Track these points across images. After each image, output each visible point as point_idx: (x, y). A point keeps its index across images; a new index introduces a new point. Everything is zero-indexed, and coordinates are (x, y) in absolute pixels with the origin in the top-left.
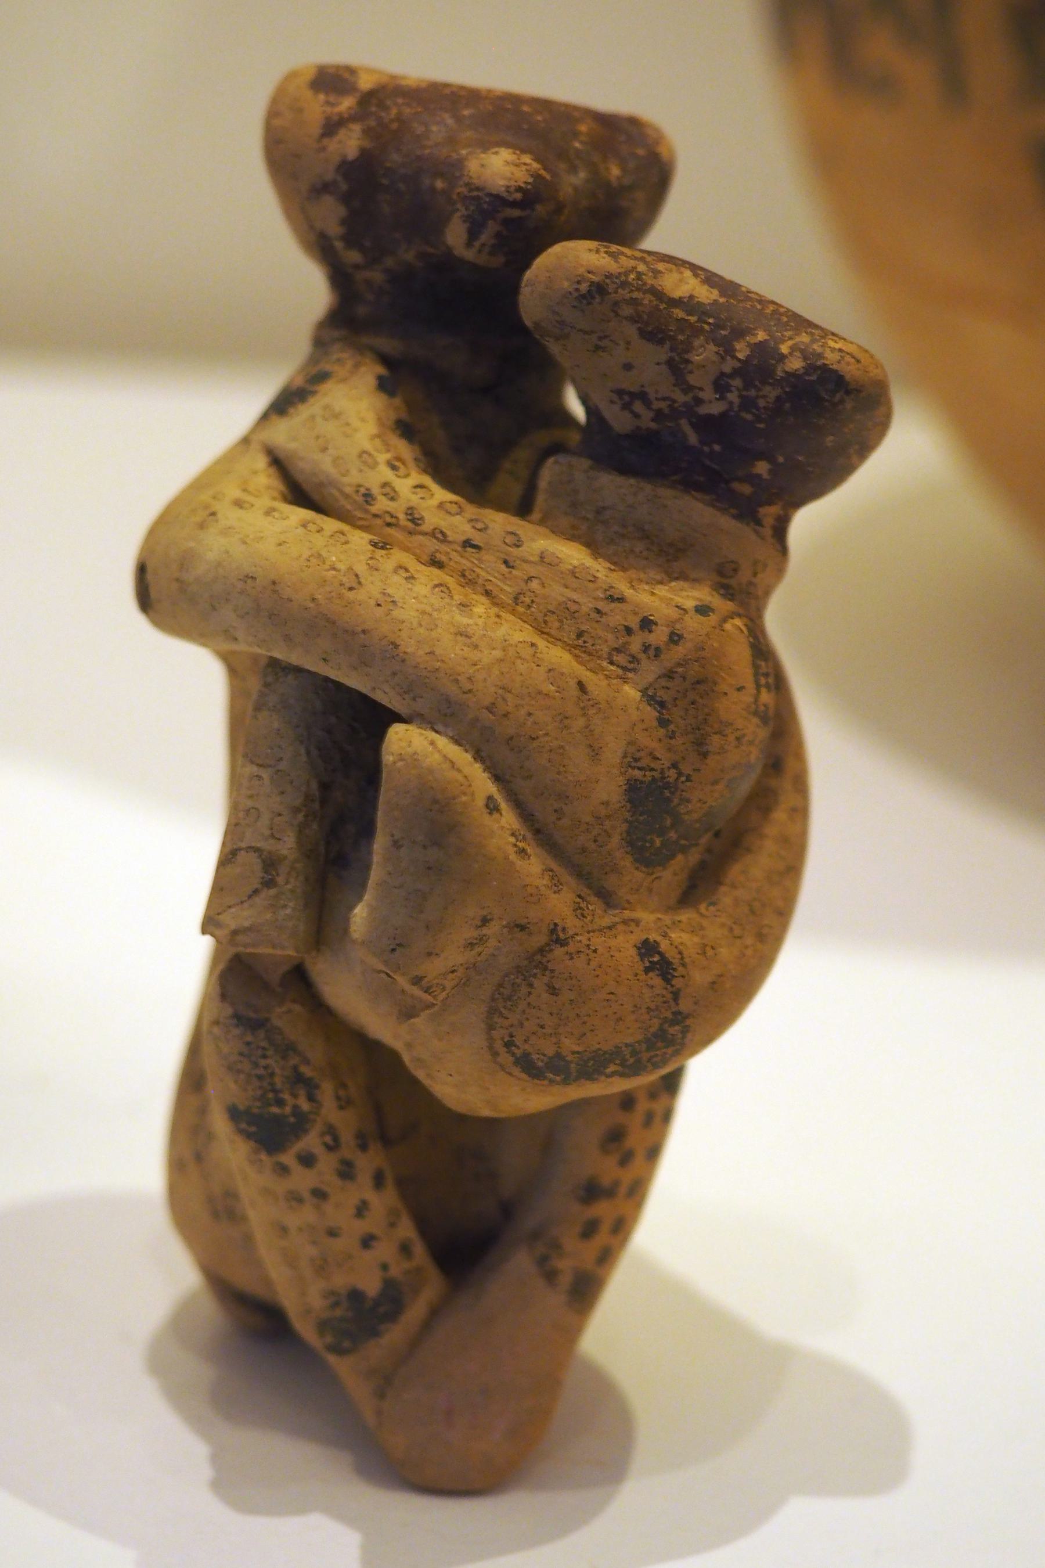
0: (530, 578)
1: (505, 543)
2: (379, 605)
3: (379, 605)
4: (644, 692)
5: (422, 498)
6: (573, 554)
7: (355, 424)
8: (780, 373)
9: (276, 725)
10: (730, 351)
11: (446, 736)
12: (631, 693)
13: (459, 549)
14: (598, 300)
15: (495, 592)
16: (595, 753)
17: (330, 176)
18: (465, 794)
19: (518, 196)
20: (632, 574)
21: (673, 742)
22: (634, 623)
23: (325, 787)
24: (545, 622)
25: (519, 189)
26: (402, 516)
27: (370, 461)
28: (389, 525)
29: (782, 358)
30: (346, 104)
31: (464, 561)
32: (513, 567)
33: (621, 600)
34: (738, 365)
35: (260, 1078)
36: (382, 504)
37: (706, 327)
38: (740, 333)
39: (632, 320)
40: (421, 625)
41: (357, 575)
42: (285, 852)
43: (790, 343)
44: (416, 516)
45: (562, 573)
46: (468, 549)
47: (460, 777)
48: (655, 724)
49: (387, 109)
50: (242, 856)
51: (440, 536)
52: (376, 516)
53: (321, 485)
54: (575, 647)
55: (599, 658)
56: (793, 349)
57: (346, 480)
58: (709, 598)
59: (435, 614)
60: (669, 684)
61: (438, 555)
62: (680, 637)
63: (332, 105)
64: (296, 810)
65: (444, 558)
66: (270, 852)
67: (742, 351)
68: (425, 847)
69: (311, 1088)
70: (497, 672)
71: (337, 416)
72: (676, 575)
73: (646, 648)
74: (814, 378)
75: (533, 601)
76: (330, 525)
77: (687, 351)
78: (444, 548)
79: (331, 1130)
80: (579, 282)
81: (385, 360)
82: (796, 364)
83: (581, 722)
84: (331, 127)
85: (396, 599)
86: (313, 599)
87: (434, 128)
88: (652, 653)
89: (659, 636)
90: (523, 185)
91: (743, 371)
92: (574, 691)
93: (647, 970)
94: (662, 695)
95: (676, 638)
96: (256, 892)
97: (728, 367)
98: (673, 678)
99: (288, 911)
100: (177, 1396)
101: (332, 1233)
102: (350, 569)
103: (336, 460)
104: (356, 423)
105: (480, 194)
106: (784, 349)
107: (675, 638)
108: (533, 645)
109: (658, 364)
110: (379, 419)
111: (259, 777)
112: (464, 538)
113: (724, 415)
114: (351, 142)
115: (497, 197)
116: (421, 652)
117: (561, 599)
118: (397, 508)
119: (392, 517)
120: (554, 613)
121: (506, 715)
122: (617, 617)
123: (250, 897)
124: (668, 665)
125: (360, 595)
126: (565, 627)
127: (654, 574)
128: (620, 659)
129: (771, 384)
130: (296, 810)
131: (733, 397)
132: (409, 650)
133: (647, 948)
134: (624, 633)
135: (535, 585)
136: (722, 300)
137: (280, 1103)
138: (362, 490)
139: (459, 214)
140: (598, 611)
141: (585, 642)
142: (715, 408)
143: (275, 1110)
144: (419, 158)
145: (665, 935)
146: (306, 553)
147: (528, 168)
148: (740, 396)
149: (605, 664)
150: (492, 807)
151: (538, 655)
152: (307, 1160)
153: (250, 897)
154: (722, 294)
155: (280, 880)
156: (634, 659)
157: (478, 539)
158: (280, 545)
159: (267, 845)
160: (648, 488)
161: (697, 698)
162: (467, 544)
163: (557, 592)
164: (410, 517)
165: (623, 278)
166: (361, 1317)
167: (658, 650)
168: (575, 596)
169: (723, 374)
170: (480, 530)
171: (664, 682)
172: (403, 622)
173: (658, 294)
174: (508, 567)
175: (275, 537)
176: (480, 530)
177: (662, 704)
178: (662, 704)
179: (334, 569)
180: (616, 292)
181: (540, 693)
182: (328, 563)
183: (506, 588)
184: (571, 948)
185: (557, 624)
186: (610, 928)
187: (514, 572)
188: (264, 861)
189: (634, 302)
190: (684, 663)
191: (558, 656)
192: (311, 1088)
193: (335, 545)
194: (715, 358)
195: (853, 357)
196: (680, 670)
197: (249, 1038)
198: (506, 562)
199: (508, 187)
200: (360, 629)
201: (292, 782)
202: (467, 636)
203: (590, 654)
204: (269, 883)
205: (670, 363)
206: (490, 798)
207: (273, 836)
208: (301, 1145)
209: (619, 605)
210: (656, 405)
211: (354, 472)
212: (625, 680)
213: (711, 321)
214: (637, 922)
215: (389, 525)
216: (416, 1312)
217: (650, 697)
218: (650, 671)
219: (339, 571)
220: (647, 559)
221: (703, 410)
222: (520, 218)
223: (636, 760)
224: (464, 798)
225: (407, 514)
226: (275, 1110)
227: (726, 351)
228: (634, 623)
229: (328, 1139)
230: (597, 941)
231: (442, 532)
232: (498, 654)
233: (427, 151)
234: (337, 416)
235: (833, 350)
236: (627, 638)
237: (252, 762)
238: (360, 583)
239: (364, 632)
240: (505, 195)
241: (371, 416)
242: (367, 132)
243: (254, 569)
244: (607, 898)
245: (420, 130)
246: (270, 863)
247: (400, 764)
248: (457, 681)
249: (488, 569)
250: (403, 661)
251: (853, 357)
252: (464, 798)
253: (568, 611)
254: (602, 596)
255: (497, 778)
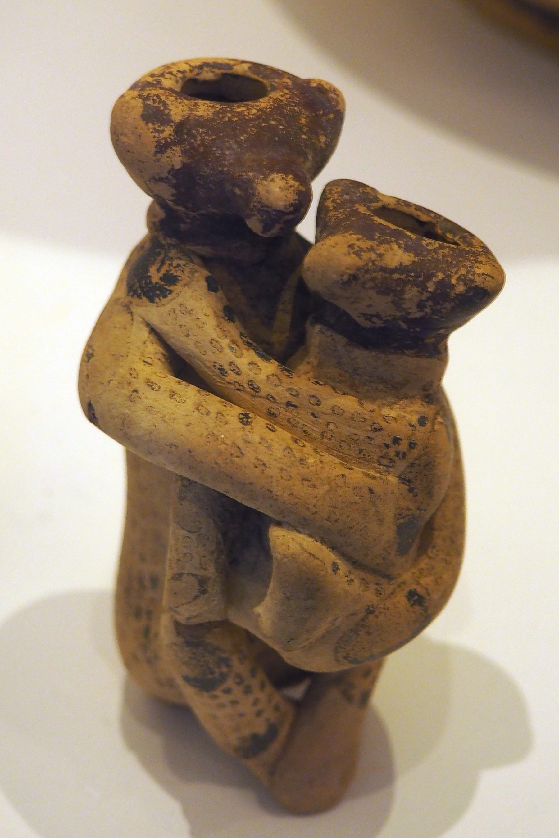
0: (329, 424)
1: (310, 403)
2: (256, 467)
3: (256, 467)
4: (399, 477)
5: (255, 374)
6: (348, 403)
7: (194, 311)
8: (453, 295)
9: (195, 510)
10: (425, 289)
11: (305, 534)
12: (393, 479)
13: (284, 407)
14: (354, 283)
15: (309, 431)
16: (381, 521)
17: (164, 175)
18: (323, 570)
19: (291, 209)
20: (379, 402)
21: (417, 498)
22: (389, 441)
23: (224, 534)
24: (341, 447)
25: (292, 205)
26: (246, 386)
27: (217, 346)
28: (238, 390)
29: (453, 286)
30: (168, 132)
31: (288, 414)
32: (317, 417)
33: (381, 429)
34: (429, 295)
35: (202, 666)
36: (232, 377)
37: (411, 279)
38: (429, 277)
39: (373, 288)
40: (282, 478)
41: (239, 448)
42: (210, 575)
43: (456, 276)
44: (255, 386)
45: (346, 419)
46: (290, 407)
47: (319, 563)
48: (408, 492)
49: (194, 137)
50: (185, 578)
51: (271, 399)
52: (229, 383)
53: (189, 355)
54: (359, 458)
55: (373, 462)
56: (458, 279)
57: (205, 357)
58: (423, 409)
59: (289, 469)
60: (413, 470)
61: (272, 410)
62: (415, 444)
63: (158, 131)
64: (212, 553)
65: (276, 412)
66: (202, 576)
67: (431, 287)
68: (304, 600)
69: (226, 662)
70: (328, 499)
71: (190, 312)
72: (402, 397)
73: (398, 454)
74: (471, 294)
75: (332, 436)
76: (213, 403)
77: (403, 294)
78: (275, 406)
79: (239, 676)
80: (342, 275)
81: (206, 261)
82: (461, 288)
83: (373, 510)
84: (162, 147)
85: (266, 463)
86: (216, 463)
87: (227, 152)
88: (401, 456)
89: (403, 446)
90: (294, 202)
91: (434, 297)
92: (368, 495)
93: (412, 606)
94: (411, 476)
95: (413, 445)
96: (197, 597)
97: (425, 296)
98: (414, 467)
99: (215, 602)
100: (147, 763)
101: (241, 715)
102: (234, 443)
103: (196, 343)
104: (203, 318)
105: (269, 209)
106: (454, 281)
107: (412, 445)
108: (343, 475)
109: (387, 303)
110: (215, 313)
111: (190, 538)
112: (286, 401)
113: (422, 318)
114: (175, 158)
115: (280, 211)
116: (285, 495)
117: (348, 434)
118: (243, 380)
119: (240, 385)
120: (345, 441)
121: (336, 521)
122: (379, 439)
123: (194, 599)
124: (410, 461)
125: (244, 461)
126: (352, 448)
127: (391, 399)
128: (385, 462)
129: (448, 302)
130: (212, 553)
131: (428, 310)
132: (278, 494)
133: (412, 594)
134: (385, 447)
135: (332, 427)
136: (416, 259)
137: (212, 673)
138: (218, 366)
139: (254, 218)
140: (369, 438)
141: (364, 455)
142: (418, 315)
143: (210, 676)
144: (221, 172)
145: (418, 584)
146: (205, 434)
147: (293, 189)
148: (432, 309)
149: (376, 465)
150: (335, 568)
151: (347, 481)
152: (228, 691)
153: (194, 599)
154: (416, 255)
155: (209, 589)
156: (392, 461)
157: (294, 401)
158: (188, 426)
159: (201, 573)
160: (383, 356)
161: (427, 473)
162: (289, 404)
163: (345, 430)
164: (251, 387)
165: (366, 268)
166: (255, 746)
167: (404, 454)
168: (356, 431)
169: (422, 300)
170: (294, 396)
171: (408, 470)
172: (272, 477)
173: (384, 269)
174: (315, 417)
175: (178, 410)
176: (294, 396)
177: (409, 481)
178: (409, 481)
179: (225, 443)
180: (363, 277)
181: (351, 503)
182: (220, 440)
183: (315, 429)
184: (376, 613)
185: (347, 447)
186: (392, 593)
187: (319, 420)
188: (199, 581)
189: (373, 279)
190: (419, 458)
191: (357, 475)
192: (226, 662)
193: (220, 426)
194: (417, 294)
195: (490, 276)
196: (417, 462)
197: (195, 650)
198: (313, 414)
199: (285, 206)
200: (247, 482)
201: (208, 539)
202: (309, 481)
203: (367, 461)
204: (204, 592)
205: (393, 302)
206: (334, 564)
207: (202, 568)
208: (225, 686)
209: (380, 433)
210: (385, 319)
211: (209, 353)
212: (388, 473)
213: (413, 274)
214: (404, 583)
215: (238, 390)
216: (283, 732)
217: (403, 480)
218: (401, 465)
219: (227, 445)
220: (386, 392)
221: (410, 317)
222: (293, 218)
223: (400, 515)
224: (323, 573)
225: (249, 385)
226: (210, 676)
227: (423, 290)
228: (389, 441)
229: (238, 680)
230: (389, 604)
231: (272, 397)
232: (326, 487)
233: (225, 169)
234: (190, 312)
235: (479, 275)
236: (387, 450)
237: (183, 528)
238: (241, 453)
239: (250, 484)
240: (285, 210)
241: (209, 311)
242: (184, 152)
243: (175, 441)
244: (389, 578)
245: (218, 153)
246: (203, 582)
247: (285, 560)
248: (308, 508)
249: (304, 419)
250: (276, 500)
251: (490, 276)
252: (323, 573)
253: (352, 440)
254: (370, 429)
255: (333, 548)
